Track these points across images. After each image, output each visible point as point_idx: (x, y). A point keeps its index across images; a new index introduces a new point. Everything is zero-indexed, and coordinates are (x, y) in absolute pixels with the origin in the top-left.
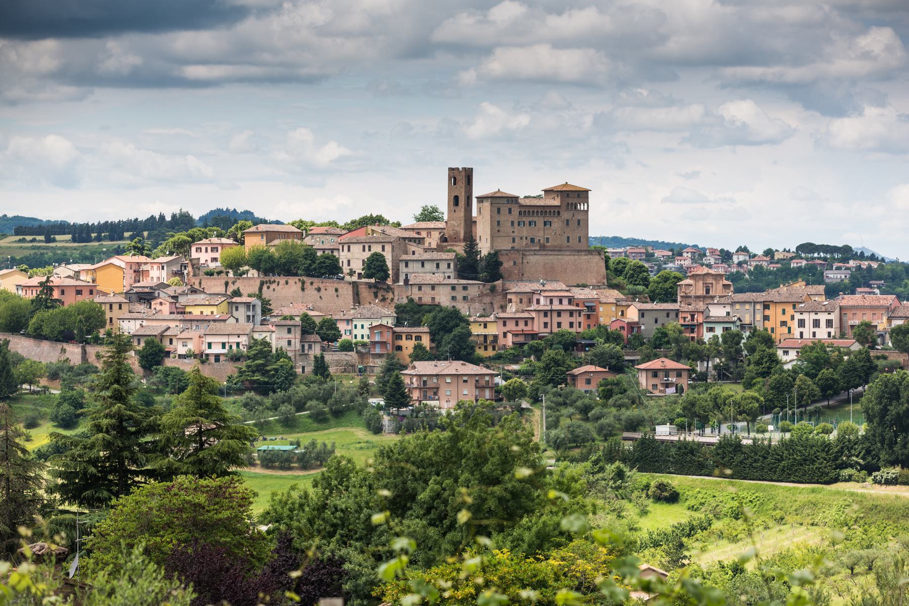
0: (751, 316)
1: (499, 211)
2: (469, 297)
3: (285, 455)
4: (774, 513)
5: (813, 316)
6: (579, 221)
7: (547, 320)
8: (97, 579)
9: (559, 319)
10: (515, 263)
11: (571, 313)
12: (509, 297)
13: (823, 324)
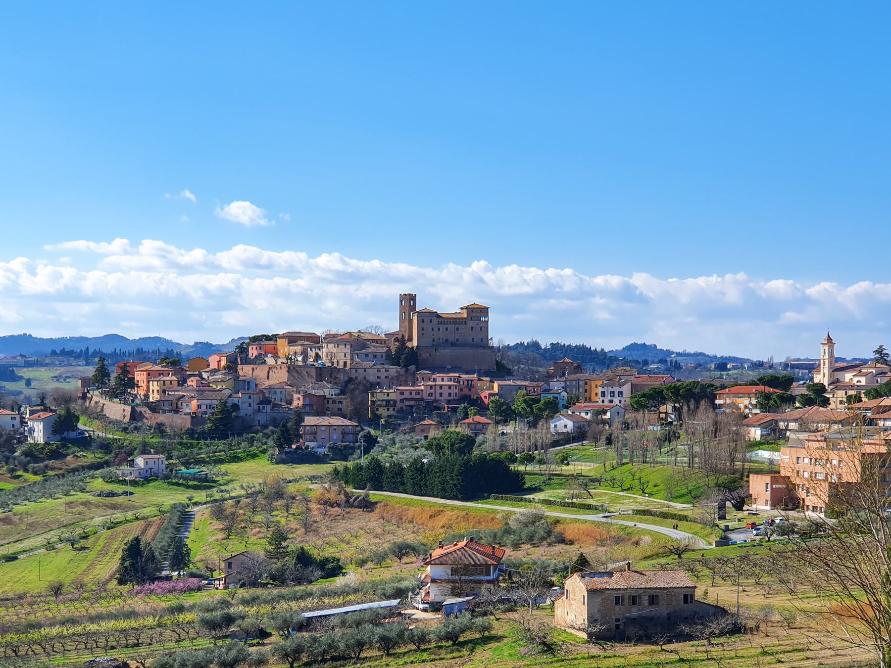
0: (576, 390)
1: (423, 321)
2: (390, 377)
3: (562, 487)
4: (253, 532)
5: (610, 389)
6: (481, 328)
7: (432, 391)
8: (423, 541)
9: (441, 391)
10: (430, 355)
11: (450, 387)
12: (823, 438)
13: (616, 394)
